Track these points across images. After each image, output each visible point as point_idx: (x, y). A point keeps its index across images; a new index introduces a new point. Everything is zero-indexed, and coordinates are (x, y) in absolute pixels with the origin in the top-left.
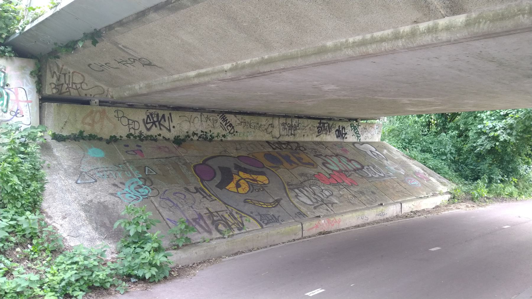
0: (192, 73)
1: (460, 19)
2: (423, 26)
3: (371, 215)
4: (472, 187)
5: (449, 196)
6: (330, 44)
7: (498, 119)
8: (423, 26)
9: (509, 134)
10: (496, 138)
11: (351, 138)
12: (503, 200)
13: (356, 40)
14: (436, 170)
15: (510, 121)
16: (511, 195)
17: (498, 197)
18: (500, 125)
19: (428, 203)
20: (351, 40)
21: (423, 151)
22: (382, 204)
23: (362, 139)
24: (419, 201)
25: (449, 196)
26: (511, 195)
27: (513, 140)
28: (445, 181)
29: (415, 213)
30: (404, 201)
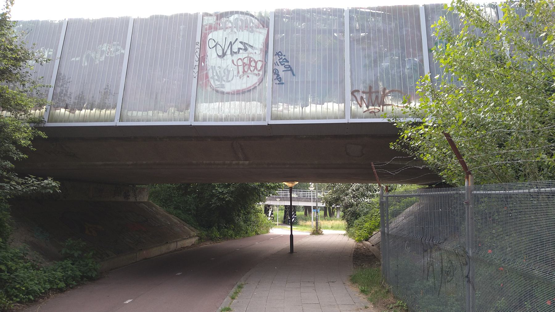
0: (101, 163)
1: (247, 162)
2: (234, 162)
3: (164, 249)
4: (209, 232)
5: (197, 238)
6: (194, 162)
7: (224, 187)
8: (234, 162)
9: (231, 197)
10: (223, 199)
11: (132, 199)
12: (228, 239)
13: (334, 225)
14: (185, 221)
15: (232, 189)
16: (231, 236)
17: (225, 237)
18: (225, 191)
19: (188, 242)
20: (205, 162)
21: (175, 208)
22: (167, 243)
23: (138, 200)
24: (184, 241)
25: (197, 238)
26: (231, 236)
27: (232, 199)
28: (193, 228)
29: (184, 248)
30: (179, 241)
